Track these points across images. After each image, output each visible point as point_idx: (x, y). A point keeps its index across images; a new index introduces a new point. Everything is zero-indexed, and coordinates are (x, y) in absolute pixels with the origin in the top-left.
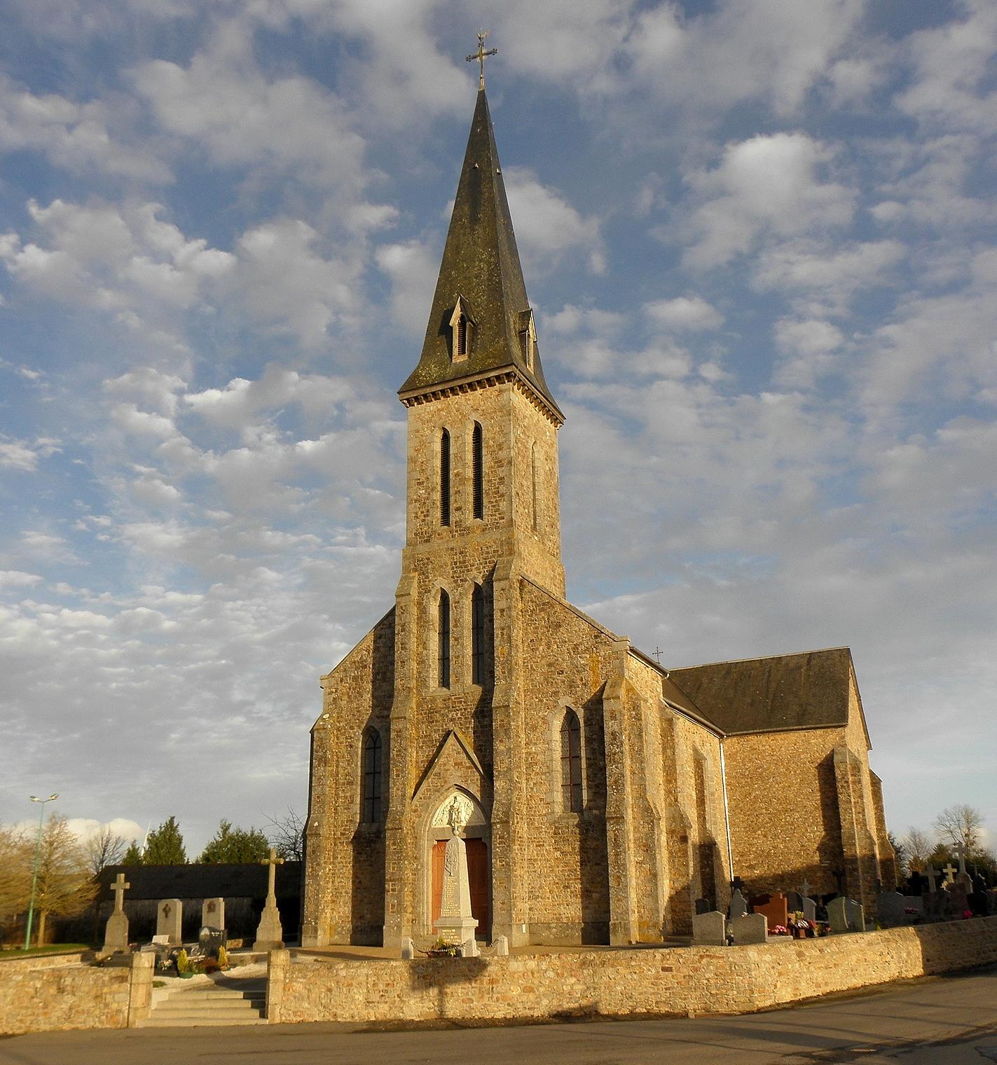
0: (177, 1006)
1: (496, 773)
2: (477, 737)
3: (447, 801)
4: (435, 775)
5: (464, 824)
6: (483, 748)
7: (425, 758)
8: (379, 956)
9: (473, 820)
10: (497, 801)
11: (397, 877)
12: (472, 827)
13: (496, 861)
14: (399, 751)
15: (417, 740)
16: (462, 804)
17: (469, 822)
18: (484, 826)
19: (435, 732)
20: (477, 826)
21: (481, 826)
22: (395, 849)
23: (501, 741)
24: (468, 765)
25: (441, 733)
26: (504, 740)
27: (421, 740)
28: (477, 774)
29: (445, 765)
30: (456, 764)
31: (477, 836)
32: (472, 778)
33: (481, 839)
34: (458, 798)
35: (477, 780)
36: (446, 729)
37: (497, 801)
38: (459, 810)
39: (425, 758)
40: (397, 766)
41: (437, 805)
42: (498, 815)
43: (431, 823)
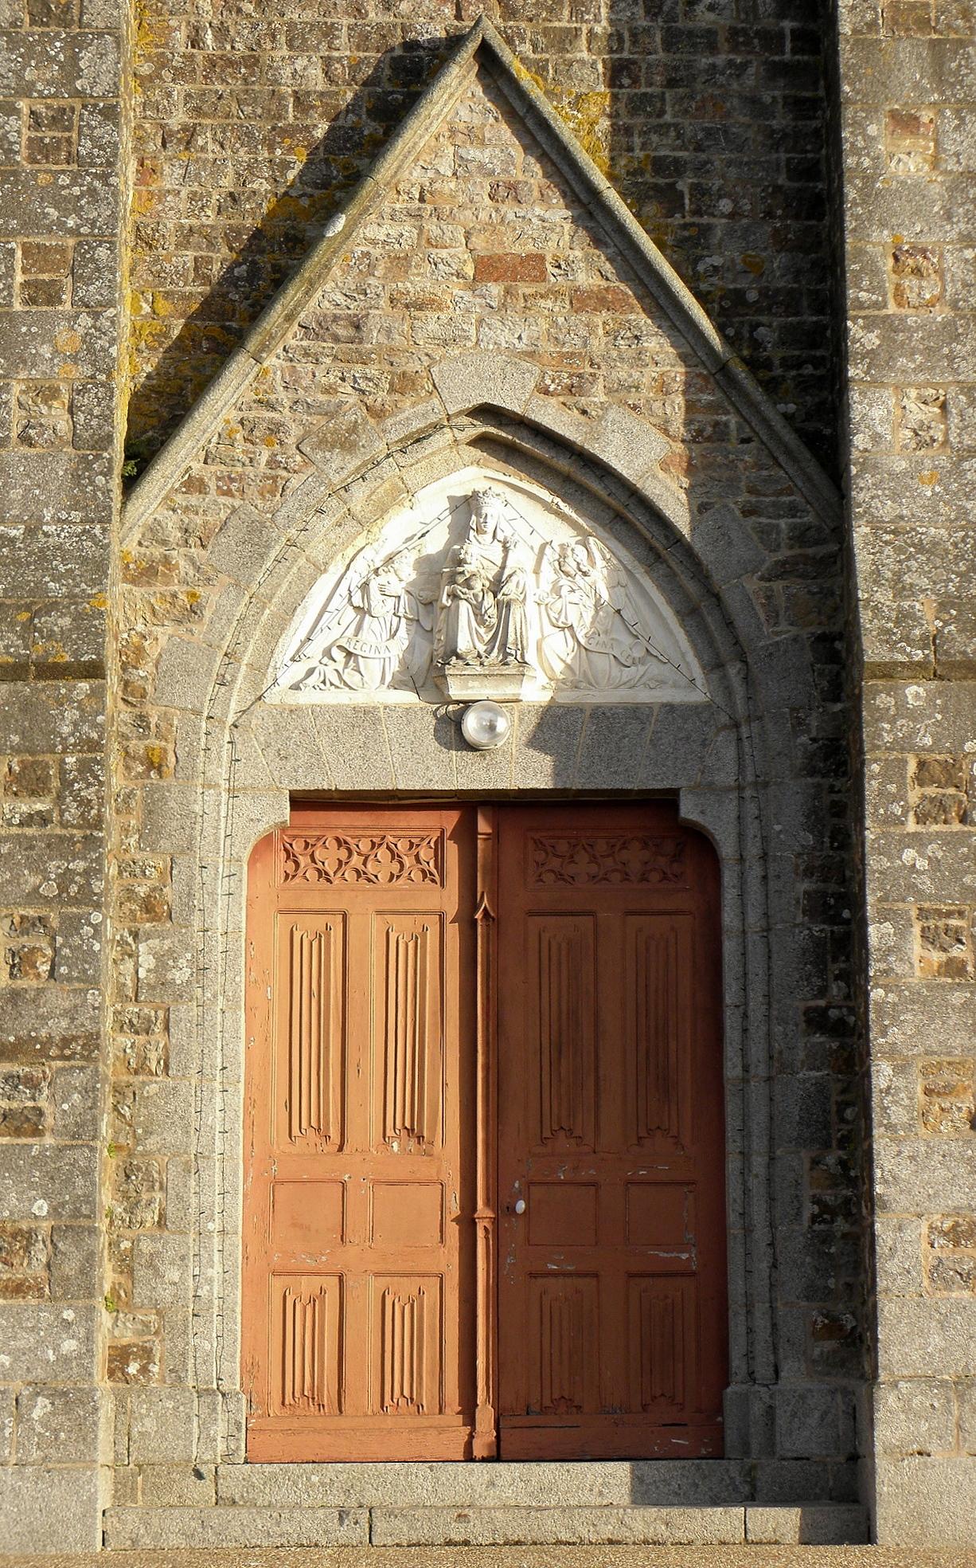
0: (758, 1314)
1: (861, 336)
2: (638, 104)
3: (396, 528)
4: (318, 330)
5: (536, 692)
6: (683, 185)
7: (210, 217)
8: (775, 956)
9: (602, 663)
10: (877, 526)
11: (58, 1027)
12: (601, 715)
13: (902, 933)
14: (59, 118)
15: (145, 82)
16: (523, 558)
17: (576, 678)
18: (694, 710)
19: (296, 41)
20: (635, 712)
21: (670, 708)
22: (44, 819)
23: (906, 122)
24: (585, 279)
25: (344, 48)
26: (926, 116)
27: (178, 90)
28: (658, 344)
29: (401, 263)
30: (488, 268)
31: (642, 778)
32: (622, 373)
33: (666, 801)
34: (493, 509)
35: (663, 389)
36: (383, 32)
37: (877, 526)
38: (510, 589)
39: (210, 217)
40: (32, 223)
41: (317, 549)
42: (904, 617)
43: (259, 670)
